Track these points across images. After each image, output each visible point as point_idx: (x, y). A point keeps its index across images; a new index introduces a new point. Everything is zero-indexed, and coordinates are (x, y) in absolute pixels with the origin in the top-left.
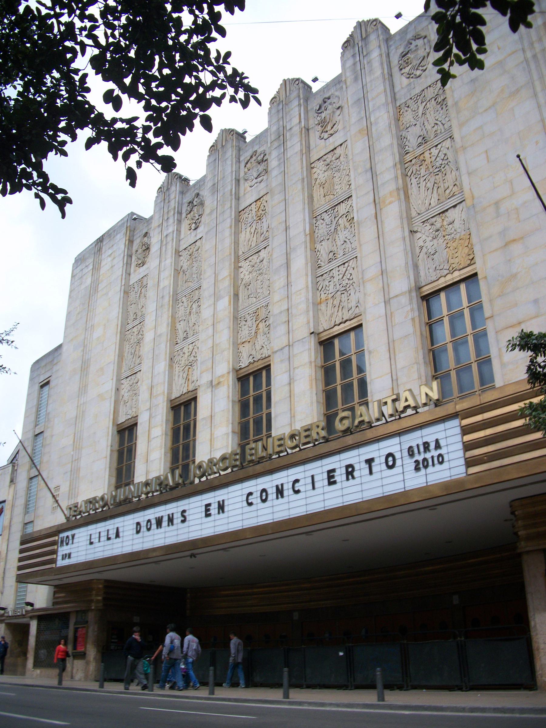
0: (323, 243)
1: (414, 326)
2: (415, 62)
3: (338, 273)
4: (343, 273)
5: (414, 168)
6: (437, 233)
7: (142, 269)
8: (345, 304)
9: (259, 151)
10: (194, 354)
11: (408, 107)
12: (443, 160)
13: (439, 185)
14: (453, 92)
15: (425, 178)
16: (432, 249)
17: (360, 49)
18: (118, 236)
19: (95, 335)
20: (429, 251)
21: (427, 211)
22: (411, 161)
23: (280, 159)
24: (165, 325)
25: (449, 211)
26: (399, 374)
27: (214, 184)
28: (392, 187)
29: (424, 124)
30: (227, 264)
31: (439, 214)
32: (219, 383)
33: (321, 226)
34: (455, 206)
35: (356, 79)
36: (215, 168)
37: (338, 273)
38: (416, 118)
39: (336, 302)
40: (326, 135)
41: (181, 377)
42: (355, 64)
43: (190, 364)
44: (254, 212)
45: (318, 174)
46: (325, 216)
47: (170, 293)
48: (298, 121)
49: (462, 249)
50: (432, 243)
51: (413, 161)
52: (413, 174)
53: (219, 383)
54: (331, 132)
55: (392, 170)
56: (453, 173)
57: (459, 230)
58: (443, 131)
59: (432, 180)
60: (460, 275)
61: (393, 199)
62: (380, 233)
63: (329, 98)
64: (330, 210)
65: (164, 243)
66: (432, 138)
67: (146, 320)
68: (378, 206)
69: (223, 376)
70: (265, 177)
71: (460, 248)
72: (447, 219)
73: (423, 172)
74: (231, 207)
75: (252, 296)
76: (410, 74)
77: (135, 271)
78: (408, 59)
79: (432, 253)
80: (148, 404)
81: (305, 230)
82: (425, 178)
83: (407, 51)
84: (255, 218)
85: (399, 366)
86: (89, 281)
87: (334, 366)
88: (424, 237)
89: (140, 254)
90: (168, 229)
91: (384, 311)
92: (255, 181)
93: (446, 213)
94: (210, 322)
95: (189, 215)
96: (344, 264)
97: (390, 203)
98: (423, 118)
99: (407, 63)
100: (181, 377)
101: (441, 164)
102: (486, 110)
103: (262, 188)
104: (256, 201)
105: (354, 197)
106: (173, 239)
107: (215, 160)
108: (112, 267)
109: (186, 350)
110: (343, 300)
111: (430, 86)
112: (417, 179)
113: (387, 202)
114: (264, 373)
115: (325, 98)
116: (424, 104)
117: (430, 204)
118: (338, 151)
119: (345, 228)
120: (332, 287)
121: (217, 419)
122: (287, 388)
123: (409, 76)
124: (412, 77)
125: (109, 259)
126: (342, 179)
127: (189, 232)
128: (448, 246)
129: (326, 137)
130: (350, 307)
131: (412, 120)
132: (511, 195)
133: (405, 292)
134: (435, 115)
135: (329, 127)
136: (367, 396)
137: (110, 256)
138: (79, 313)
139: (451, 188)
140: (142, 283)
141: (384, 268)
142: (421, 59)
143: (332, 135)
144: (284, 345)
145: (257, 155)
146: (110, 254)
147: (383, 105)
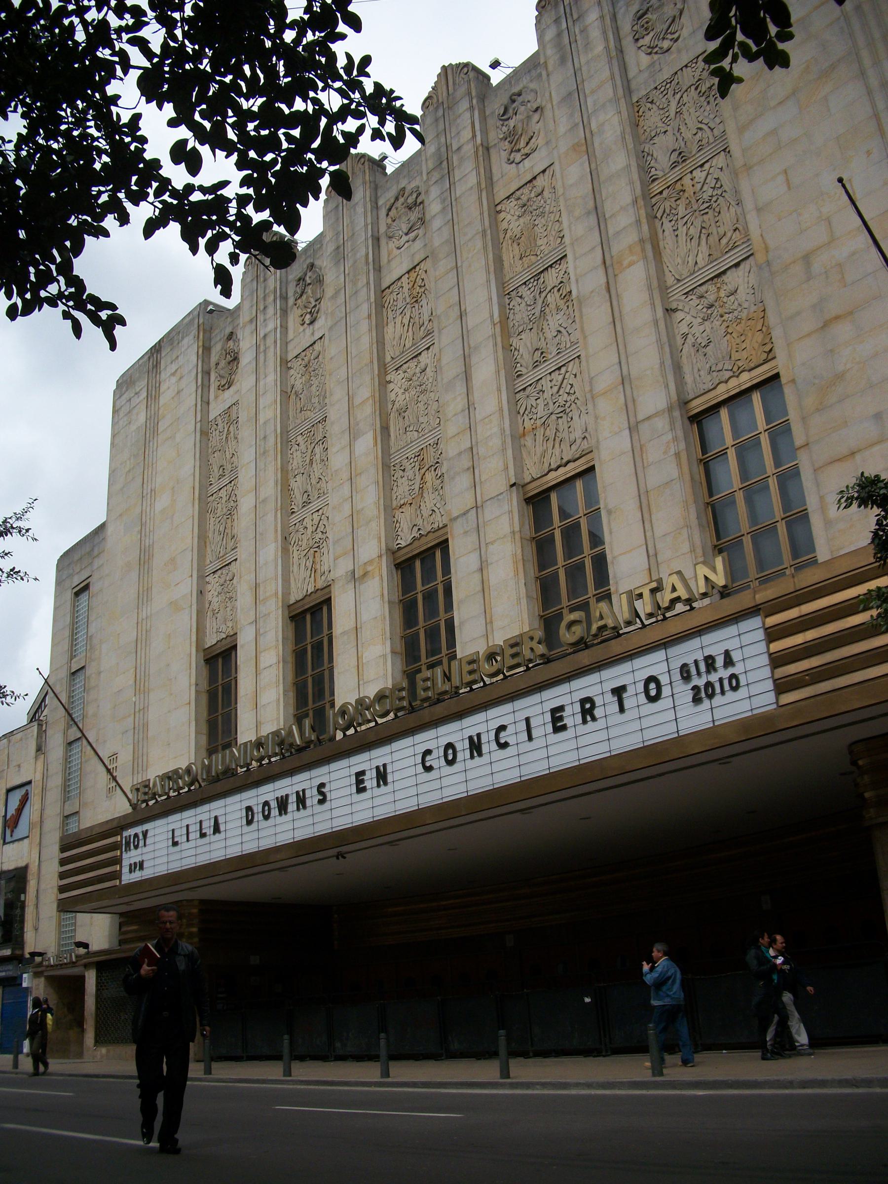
1: (679, 465)
3: (549, 384)
5: (667, 204)
7: (228, 393)
8: (565, 435)
10: (321, 528)
11: (652, 102)
12: (714, 188)
13: (710, 231)
16: (702, 338)
18: (186, 341)
20: (699, 341)
21: (691, 274)
22: (661, 193)
24: (271, 483)
25: (729, 273)
28: (632, 237)
29: (679, 129)
30: (367, 378)
31: (712, 279)
32: (365, 574)
33: (517, 308)
34: (737, 265)
35: (563, 60)
37: (549, 384)
39: (550, 433)
40: (518, 157)
42: (559, 35)
43: (317, 545)
45: (509, 223)
46: (523, 291)
49: (753, 336)
50: (702, 328)
51: (665, 194)
52: (665, 215)
53: (365, 574)
54: (527, 150)
55: (631, 211)
57: (745, 305)
58: (711, 140)
59: (698, 223)
60: (751, 379)
61: (635, 258)
64: (532, 280)
65: (262, 348)
66: (694, 153)
69: (371, 562)
70: (421, 232)
73: (681, 211)
74: (368, 283)
75: (411, 429)
76: (653, 48)
77: (216, 397)
78: (647, 23)
79: (703, 345)
81: (492, 316)
86: (142, 418)
88: (689, 318)
90: (266, 326)
91: (630, 445)
92: (405, 238)
93: (724, 278)
94: (345, 475)
95: (299, 301)
97: (630, 265)
99: (646, 29)
101: (712, 196)
102: (780, 103)
104: (408, 272)
105: (570, 257)
106: (275, 342)
107: (337, 207)
108: (178, 392)
109: (308, 522)
111: (686, 66)
112: (673, 222)
113: (626, 263)
115: (514, 94)
116: (678, 96)
117: (696, 263)
118: (539, 182)
122: (477, 577)
123: (651, 50)
124: (656, 53)
125: (174, 380)
126: (549, 228)
127: (302, 328)
129: (517, 160)
131: (660, 124)
132: (829, 243)
133: (663, 411)
134: (698, 114)
135: (522, 144)
137: (173, 374)
138: (129, 471)
139: (729, 234)
140: (230, 416)
147: (610, 101)
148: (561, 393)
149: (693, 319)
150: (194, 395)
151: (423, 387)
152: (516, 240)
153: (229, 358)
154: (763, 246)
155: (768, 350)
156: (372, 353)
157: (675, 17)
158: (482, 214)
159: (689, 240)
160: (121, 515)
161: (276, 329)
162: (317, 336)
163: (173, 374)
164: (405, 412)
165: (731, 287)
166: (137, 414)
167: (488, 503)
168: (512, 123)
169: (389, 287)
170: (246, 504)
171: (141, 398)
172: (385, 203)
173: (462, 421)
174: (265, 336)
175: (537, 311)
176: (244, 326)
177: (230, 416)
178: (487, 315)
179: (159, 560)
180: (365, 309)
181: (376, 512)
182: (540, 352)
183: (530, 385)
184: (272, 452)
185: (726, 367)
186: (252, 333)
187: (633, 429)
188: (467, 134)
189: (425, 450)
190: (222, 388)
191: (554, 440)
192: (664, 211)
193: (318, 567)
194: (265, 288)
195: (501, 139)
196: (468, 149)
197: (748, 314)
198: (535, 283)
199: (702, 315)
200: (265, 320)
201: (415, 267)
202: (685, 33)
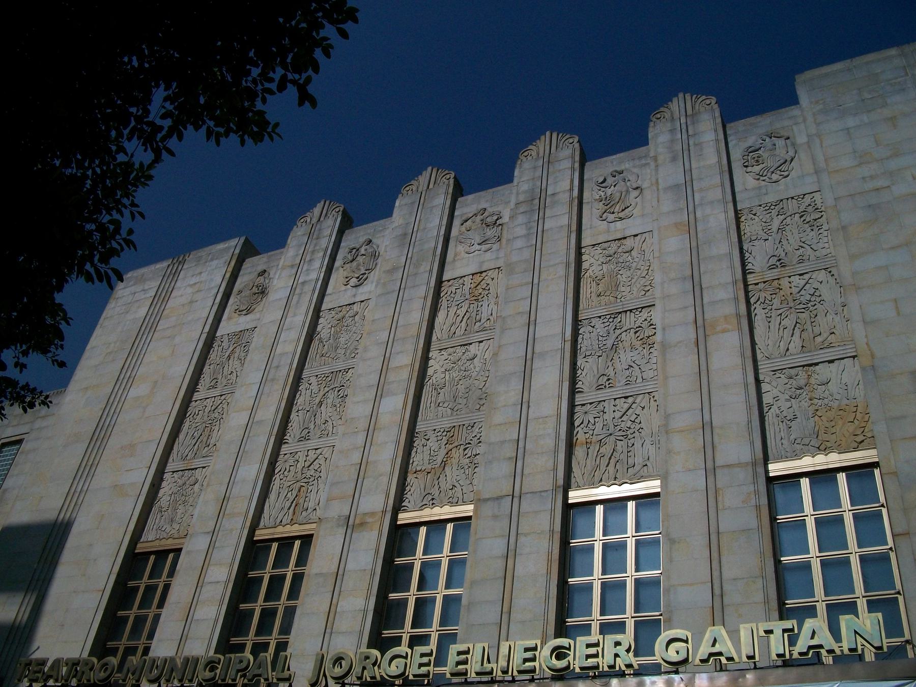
0: (590, 359)
1: (759, 516)
2: (771, 163)
3: (613, 408)
4: (624, 410)
5: (763, 295)
6: (798, 392)
7: (243, 319)
9: (490, 210)
10: (316, 465)
11: (755, 215)
14: (838, 212)
15: (780, 312)
17: (684, 126)
18: (215, 262)
19: (133, 393)
20: (785, 414)
22: (756, 284)
23: (530, 229)
24: (273, 409)
26: (726, 587)
27: (405, 234)
30: (410, 347)
31: (803, 366)
32: (362, 524)
35: (674, 159)
36: (411, 213)
37: (613, 408)
38: (768, 231)
39: (607, 450)
40: (611, 217)
41: (282, 496)
43: (305, 480)
44: (466, 288)
45: (591, 265)
46: (597, 323)
47: (291, 364)
48: (569, 188)
49: (844, 424)
50: (788, 404)
51: (761, 286)
52: (759, 303)
53: (362, 524)
55: (730, 289)
56: (830, 317)
59: (793, 317)
62: (703, 368)
63: (621, 173)
64: (608, 317)
65: (298, 291)
67: (237, 395)
68: (701, 332)
69: (373, 514)
70: (495, 247)
71: (840, 422)
72: (817, 377)
73: (776, 303)
74: (431, 271)
75: (445, 405)
77: (229, 318)
80: (212, 524)
81: (564, 334)
82: (780, 312)
83: (757, 147)
84: (468, 296)
85: (726, 574)
86: (143, 312)
87: (262, 578)
89: (245, 297)
90: (308, 275)
92: (478, 247)
94: (363, 424)
95: (348, 265)
96: (626, 397)
97: (724, 331)
98: (780, 234)
100: (282, 496)
102: (892, 248)
103: (489, 259)
104: (473, 275)
105: (659, 306)
106: (314, 290)
107: (413, 203)
108: (191, 302)
109: (301, 457)
110: (619, 448)
111: (792, 198)
113: (719, 328)
114: (171, 556)
115: (616, 171)
116: (783, 217)
117: (788, 349)
118: (629, 243)
119: (632, 348)
120: (599, 426)
121: (349, 583)
122: (500, 563)
125: (189, 290)
126: (633, 281)
127: (344, 288)
128: (819, 413)
129: (609, 220)
130: (631, 461)
131: (761, 232)
134: (801, 235)
136: (289, 634)
137: (191, 286)
138: (110, 353)
139: (825, 335)
140: (241, 339)
141: (707, 417)
142: (782, 161)
143: (621, 219)
144: (504, 493)
145: (486, 214)
146: (192, 283)
147: (719, 201)
148: (624, 418)
149: (779, 394)
150: (208, 309)
151: (467, 373)
152: (597, 280)
153: (255, 290)
154: (869, 352)
155: (859, 441)
156: (420, 328)
157: (786, 161)
158: (568, 249)
159: (782, 329)
160: (87, 388)
161: (317, 280)
162: (358, 299)
163: (191, 286)
164: (441, 389)
165: (822, 378)
166: (139, 307)
167: (528, 495)
168: (609, 191)
169: (449, 281)
170: (236, 420)
171: (148, 295)
172: (462, 215)
173: (512, 414)
174: (304, 283)
175: (609, 343)
176: (283, 268)
177: (241, 339)
178: (559, 330)
179: (115, 442)
180: (422, 291)
181: (388, 468)
182: (606, 378)
183: (591, 404)
184: (282, 382)
185: (812, 443)
186: (290, 276)
187: (711, 471)
188: (566, 185)
189: (457, 428)
190: (239, 311)
191: (610, 459)
192: (759, 299)
193: (301, 501)
194: (315, 245)
195: (596, 200)
196: (565, 197)
197: (839, 405)
198: (611, 320)
199: (790, 394)
200: (307, 270)
201: (481, 273)
202: (793, 174)
